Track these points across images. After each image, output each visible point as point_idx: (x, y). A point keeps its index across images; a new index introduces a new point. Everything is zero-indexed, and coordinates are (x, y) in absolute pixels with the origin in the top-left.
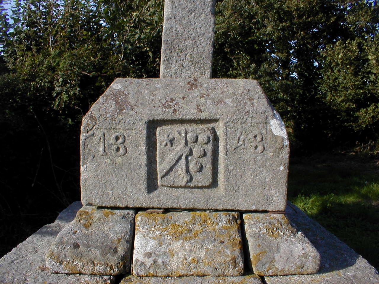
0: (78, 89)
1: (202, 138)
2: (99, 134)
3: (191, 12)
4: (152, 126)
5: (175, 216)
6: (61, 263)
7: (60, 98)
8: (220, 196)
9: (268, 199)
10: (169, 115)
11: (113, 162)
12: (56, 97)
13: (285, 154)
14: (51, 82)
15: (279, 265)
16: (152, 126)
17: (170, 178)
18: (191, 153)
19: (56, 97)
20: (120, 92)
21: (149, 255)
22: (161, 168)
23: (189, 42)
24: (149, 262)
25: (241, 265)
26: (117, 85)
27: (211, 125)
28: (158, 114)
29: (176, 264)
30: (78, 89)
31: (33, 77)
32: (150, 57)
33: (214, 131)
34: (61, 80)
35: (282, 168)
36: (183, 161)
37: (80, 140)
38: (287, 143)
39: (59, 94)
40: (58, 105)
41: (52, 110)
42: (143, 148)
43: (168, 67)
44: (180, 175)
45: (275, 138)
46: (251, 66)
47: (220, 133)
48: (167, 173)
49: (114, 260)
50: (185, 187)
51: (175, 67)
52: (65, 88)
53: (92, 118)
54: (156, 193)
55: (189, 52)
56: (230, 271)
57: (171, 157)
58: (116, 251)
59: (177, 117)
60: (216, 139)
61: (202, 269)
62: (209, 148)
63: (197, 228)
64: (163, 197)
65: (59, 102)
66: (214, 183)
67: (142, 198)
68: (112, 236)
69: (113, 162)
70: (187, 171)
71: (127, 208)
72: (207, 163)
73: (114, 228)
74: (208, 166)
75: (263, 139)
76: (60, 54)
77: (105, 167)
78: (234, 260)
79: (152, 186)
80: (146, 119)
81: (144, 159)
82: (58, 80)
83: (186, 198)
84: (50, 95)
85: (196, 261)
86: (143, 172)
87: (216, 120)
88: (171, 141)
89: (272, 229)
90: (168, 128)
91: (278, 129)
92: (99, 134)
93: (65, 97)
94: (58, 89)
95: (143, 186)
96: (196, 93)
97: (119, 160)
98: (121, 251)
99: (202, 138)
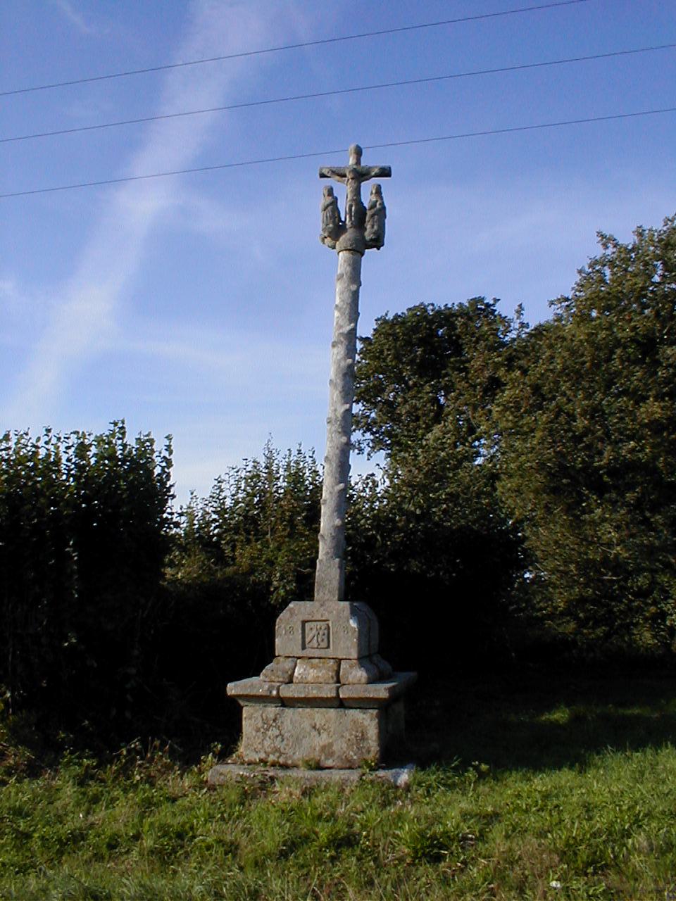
0: (294, 585)
1: (323, 628)
2: (283, 626)
3: (328, 567)
4: (304, 622)
5: (313, 661)
6: (266, 677)
7: (278, 593)
8: (330, 653)
9: (350, 654)
10: (310, 618)
11: (288, 638)
12: (274, 591)
13: (356, 634)
14: (269, 576)
15: (350, 679)
16: (304, 622)
17: (311, 644)
18: (319, 634)
19: (274, 591)
20: (293, 608)
21: (300, 674)
22: (307, 640)
23: (327, 582)
24: (300, 677)
25: (335, 679)
26: (291, 605)
27: (327, 622)
28: (306, 618)
29: (310, 678)
30: (294, 585)
31: (252, 570)
32: (377, 540)
33: (328, 625)
34: (278, 575)
35: (355, 640)
36: (316, 638)
37: (275, 625)
38: (357, 630)
39: (276, 588)
40: (275, 600)
41: (269, 603)
42: (300, 631)
43: (318, 594)
44: (315, 643)
45: (352, 628)
46: (596, 511)
47: (330, 625)
48: (309, 642)
49: (286, 676)
50: (317, 648)
51: (321, 594)
52: (282, 584)
53: (280, 619)
54: (305, 651)
55: (328, 586)
56: (331, 681)
57: (311, 635)
58: (287, 672)
59: (313, 619)
60: (329, 628)
61: (320, 680)
62: (326, 632)
63: (321, 665)
64: (308, 652)
65: (277, 597)
66: (328, 647)
67: (300, 653)
68: (287, 667)
69: (288, 638)
70: (318, 641)
71: (294, 657)
72: (325, 638)
73: (288, 664)
74: (326, 640)
75: (347, 628)
76: (279, 549)
77: (285, 639)
78: (332, 677)
79: (304, 647)
80: (301, 620)
81: (300, 636)
82: (275, 575)
83: (317, 653)
84: (268, 590)
85: (318, 677)
86: (300, 642)
87: (328, 620)
88: (311, 629)
89: (351, 667)
90: (310, 623)
91: (353, 624)
92: (283, 626)
93: (282, 592)
94: (275, 583)
95: (300, 648)
96: (322, 609)
97: (291, 637)
98: (289, 673)
99: (323, 628)
